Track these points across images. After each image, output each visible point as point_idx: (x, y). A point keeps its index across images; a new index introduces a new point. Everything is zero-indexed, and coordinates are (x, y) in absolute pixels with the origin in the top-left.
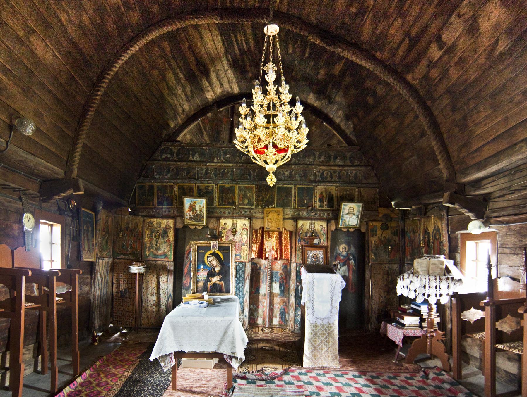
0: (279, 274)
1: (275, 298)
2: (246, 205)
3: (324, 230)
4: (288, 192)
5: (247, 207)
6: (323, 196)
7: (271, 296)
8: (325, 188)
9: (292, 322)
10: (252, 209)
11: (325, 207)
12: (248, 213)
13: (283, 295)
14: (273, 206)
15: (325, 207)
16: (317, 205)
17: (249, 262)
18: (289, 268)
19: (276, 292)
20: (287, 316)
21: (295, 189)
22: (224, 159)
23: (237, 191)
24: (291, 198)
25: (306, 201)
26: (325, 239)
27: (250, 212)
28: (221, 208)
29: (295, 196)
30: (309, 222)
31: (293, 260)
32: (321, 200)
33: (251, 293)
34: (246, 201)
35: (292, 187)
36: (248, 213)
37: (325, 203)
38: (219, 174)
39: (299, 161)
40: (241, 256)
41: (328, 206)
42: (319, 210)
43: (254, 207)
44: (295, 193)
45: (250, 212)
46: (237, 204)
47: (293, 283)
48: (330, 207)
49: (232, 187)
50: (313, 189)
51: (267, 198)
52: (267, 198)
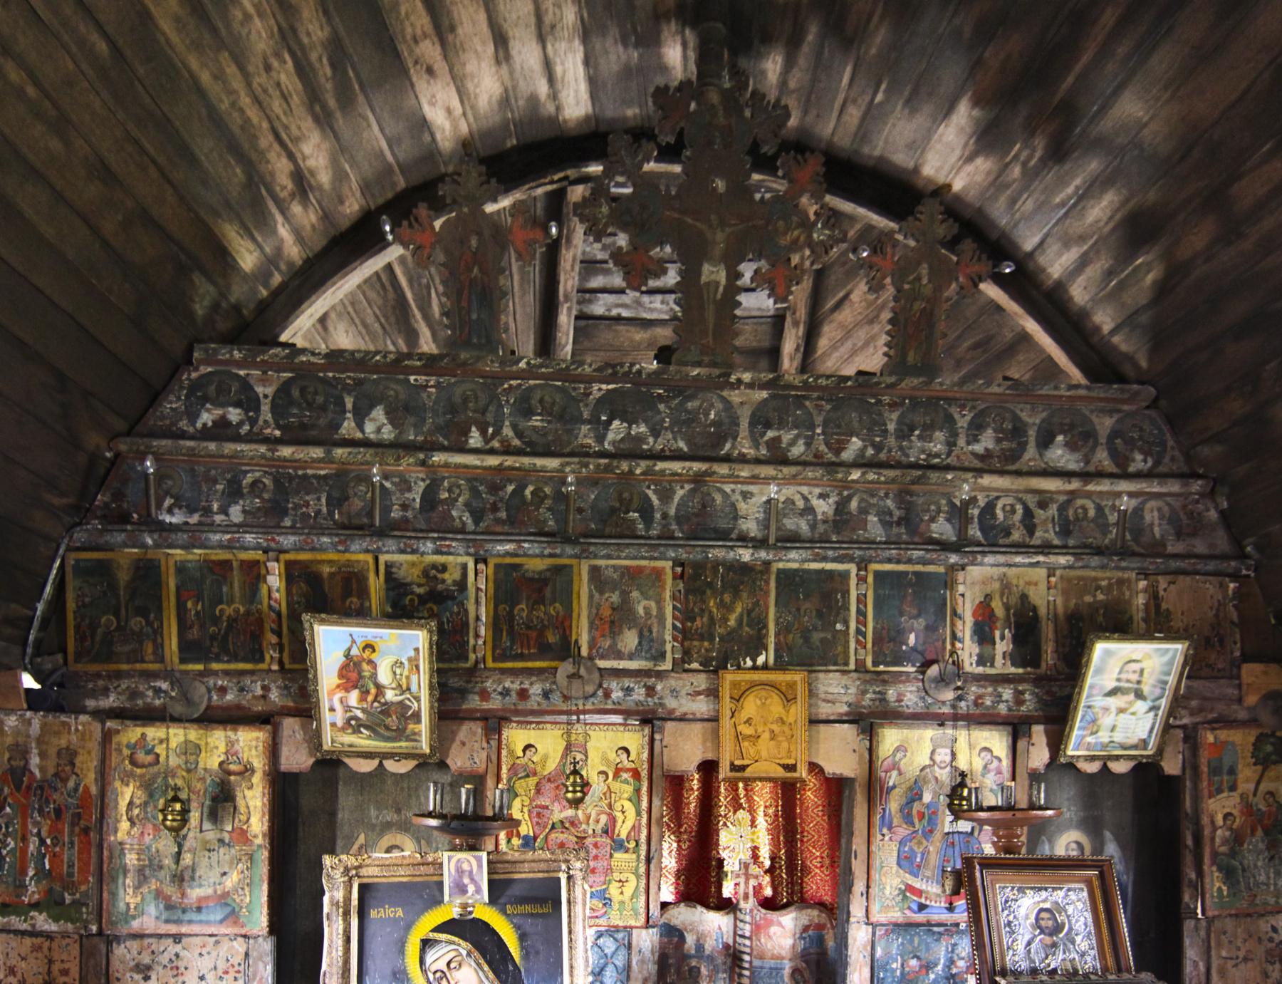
2: (631, 657)
3: (999, 772)
4: (827, 591)
10: (660, 675)
11: (1002, 666)
12: (639, 694)
15: (1002, 666)
23: (583, 587)
24: (846, 623)
27: (651, 691)
28: (503, 671)
29: (861, 613)
31: (857, 910)
32: (983, 635)
34: (630, 640)
37: (1002, 646)
38: (495, 509)
39: (878, 448)
42: (978, 678)
43: (667, 665)
44: (861, 600)
45: (651, 691)
46: (584, 652)
48: (1024, 666)
50: (948, 581)
51: (732, 623)
52: (732, 623)
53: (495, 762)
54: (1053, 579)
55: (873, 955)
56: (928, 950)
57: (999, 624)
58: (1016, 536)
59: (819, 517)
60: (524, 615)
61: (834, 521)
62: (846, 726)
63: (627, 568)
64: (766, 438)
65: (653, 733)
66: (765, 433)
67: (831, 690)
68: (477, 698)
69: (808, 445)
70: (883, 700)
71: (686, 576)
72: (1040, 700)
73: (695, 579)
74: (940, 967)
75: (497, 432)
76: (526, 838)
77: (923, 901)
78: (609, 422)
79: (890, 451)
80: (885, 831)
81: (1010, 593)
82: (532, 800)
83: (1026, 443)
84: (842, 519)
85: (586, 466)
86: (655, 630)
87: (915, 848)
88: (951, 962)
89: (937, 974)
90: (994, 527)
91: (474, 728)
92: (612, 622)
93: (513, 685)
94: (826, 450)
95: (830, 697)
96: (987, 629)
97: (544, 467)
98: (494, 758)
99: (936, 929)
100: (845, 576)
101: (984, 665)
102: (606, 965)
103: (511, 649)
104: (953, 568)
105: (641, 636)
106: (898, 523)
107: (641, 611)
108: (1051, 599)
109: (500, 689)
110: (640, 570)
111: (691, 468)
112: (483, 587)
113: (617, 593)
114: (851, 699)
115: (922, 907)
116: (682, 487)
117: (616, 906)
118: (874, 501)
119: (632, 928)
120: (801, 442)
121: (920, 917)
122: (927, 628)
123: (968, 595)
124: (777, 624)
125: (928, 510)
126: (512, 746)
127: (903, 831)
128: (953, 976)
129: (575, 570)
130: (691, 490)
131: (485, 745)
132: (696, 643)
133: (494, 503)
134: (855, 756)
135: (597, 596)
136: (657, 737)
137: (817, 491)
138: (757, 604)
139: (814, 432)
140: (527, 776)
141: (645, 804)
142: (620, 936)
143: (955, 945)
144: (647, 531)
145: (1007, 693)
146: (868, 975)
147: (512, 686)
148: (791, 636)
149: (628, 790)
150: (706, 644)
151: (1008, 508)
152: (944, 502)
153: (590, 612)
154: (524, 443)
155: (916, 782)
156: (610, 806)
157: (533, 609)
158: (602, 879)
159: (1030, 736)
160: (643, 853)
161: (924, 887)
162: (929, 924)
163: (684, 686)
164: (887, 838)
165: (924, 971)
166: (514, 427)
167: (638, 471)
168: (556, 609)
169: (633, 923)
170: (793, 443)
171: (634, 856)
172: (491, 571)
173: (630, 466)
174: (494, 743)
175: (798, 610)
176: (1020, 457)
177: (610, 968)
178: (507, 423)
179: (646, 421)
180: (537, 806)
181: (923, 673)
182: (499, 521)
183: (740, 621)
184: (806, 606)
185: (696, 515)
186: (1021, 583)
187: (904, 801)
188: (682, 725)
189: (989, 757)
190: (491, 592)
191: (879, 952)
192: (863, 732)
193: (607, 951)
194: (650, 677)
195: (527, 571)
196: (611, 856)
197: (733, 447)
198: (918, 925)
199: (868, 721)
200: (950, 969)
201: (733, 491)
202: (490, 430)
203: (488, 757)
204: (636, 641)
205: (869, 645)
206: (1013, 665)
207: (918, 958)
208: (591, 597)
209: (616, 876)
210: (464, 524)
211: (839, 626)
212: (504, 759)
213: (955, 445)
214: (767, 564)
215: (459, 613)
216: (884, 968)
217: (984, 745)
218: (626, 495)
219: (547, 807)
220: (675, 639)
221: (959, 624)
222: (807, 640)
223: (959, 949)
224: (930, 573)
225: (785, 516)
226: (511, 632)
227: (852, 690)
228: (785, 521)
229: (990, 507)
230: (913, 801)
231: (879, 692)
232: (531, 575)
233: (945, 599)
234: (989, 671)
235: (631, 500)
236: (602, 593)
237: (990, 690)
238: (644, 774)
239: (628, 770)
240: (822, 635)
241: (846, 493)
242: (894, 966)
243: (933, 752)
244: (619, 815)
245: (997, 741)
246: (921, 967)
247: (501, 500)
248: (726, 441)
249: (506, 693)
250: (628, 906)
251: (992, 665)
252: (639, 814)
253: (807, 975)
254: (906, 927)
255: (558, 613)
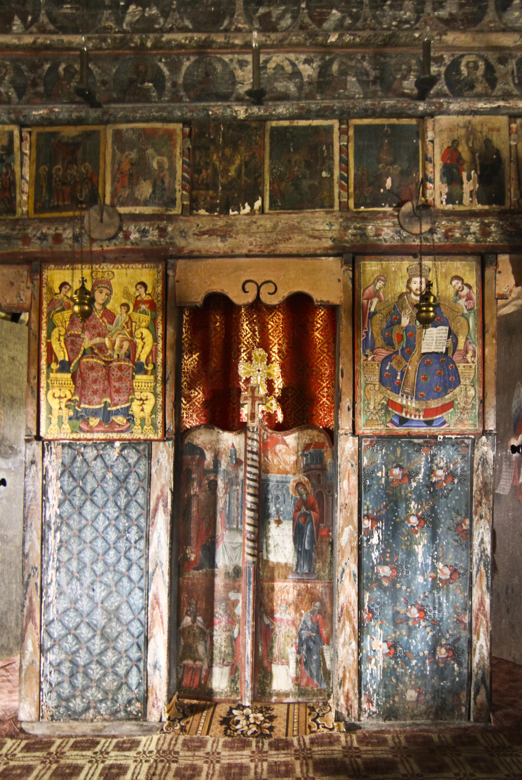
0: (291, 485)
1: (278, 585)
2: (146, 203)
3: (469, 298)
4: (314, 146)
5: (148, 210)
6: (459, 158)
7: (262, 576)
8: (467, 126)
9: (348, 685)
10: (171, 219)
11: (469, 203)
12: (153, 235)
13: (311, 572)
14: (258, 204)
15: (469, 203)
16: (437, 192)
17: (164, 439)
18: (329, 460)
19: (282, 560)
20: (327, 656)
21: (343, 132)
22: (53, 20)
23: (108, 149)
24: (331, 171)
25: (389, 183)
26: (475, 335)
27: (163, 232)
28: (41, 220)
29: (344, 162)
30: (406, 264)
31: (345, 425)
32: (452, 176)
33: (178, 566)
34: (145, 189)
35: (330, 128)
36: (153, 235)
37: (469, 186)
38: (35, 84)
39: (355, 18)
40: (131, 419)
41: (481, 196)
42: (447, 214)
43: (177, 211)
44: (343, 150)
45: (163, 232)
46: (108, 201)
47: (348, 521)
48: (490, 203)
49: (87, 135)
50: (420, 133)
51: (232, 173)
52: (232, 173)
53: (38, 298)
54: (514, 126)
55: (360, 464)
56: (409, 459)
57: (465, 166)
58: (479, 88)
59: (306, 80)
60: (60, 173)
61: (318, 83)
62: (331, 259)
63: (144, 130)
64: (258, 15)
65: (166, 269)
66: (257, 10)
67: (317, 227)
68: (20, 243)
69: (294, 18)
70: (364, 235)
71: (193, 134)
72: (505, 232)
73: (201, 136)
74: (421, 476)
75: (35, 19)
76: (63, 362)
77: (404, 415)
78: (126, 7)
79: (365, 20)
80: (368, 352)
81: (475, 138)
82: (67, 331)
83: (486, 7)
84: (324, 83)
85: (105, 40)
86: (167, 181)
87: (395, 367)
88: (430, 472)
89: (418, 482)
90: (459, 82)
91: (21, 271)
92: (131, 175)
93: (49, 230)
94: (310, 22)
95: (316, 233)
96: (455, 170)
97: (70, 43)
98: (37, 295)
99: (416, 441)
100: (329, 130)
101: (454, 203)
102: (130, 473)
103: (50, 202)
104: (422, 117)
105: (154, 186)
106: (374, 82)
107: (155, 165)
108: (513, 143)
109: (38, 235)
110: (154, 131)
111: (192, 38)
112: (27, 152)
113: (135, 151)
114: (335, 234)
115: (403, 421)
116: (188, 59)
117: (138, 422)
118: (353, 63)
119: (151, 441)
120: (288, 16)
121: (401, 430)
122: (402, 173)
123: (436, 141)
124: (271, 174)
125: (400, 70)
126: (51, 284)
127: (384, 353)
128: (433, 484)
129: (102, 134)
130: (196, 62)
131: (29, 285)
132: (202, 192)
133: (34, 79)
134: (340, 286)
135: (118, 154)
136: (170, 273)
137: (303, 57)
138: (253, 156)
139: (299, 7)
140: (63, 310)
141: (160, 332)
142: (141, 447)
143: (434, 455)
144: (160, 98)
145: (474, 226)
146: (356, 482)
147: (48, 232)
148: (283, 185)
149: (146, 319)
150: (211, 192)
151: (471, 65)
152: (414, 62)
153: (113, 167)
154: (56, 27)
155: (394, 308)
156: (131, 334)
157: (67, 168)
158: (126, 397)
159: (497, 265)
160: (160, 375)
161: (404, 402)
162: (409, 436)
163: (190, 228)
164: (370, 358)
165: (406, 480)
166: (49, 14)
167: (149, 44)
168: (85, 168)
169: (152, 436)
170: (281, 17)
171: (152, 377)
172: (34, 137)
173: (141, 39)
174: (36, 283)
175: (289, 161)
176: (480, 20)
177: (133, 476)
178: (43, 12)
179: (157, 5)
180: (71, 335)
181: (398, 211)
182: (37, 94)
183: (239, 171)
184: (296, 157)
185: (201, 83)
186: (485, 129)
187: (385, 325)
188: (190, 262)
189: (460, 284)
190: (34, 155)
191: (365, 461)
192: (346, 263)
193: (131, 461)
194: (162, 220)
195: (63, 137)
196: (133, 378)
197: (231, 23)
198: (399, 437)
199: (353, 253)
200: (430, 478)
201: (231, 60)
202: (30, 18)
203: (32, 295)
204: (150, 190)
205: (351, 190)
206: (479, 202)
207: (401, 468)
208: (114, 155)
209: (137, 395)
210: (9, 98)
211: (324, 174)
212: (44, 296)
213: (423, 12)
214: (262, 120)
215: (7, 173)
216: (371, 475)
217: (454, 274)
218: (142, 68)
219: (79, 336)
220: (183, 188)
221: (430, 166)
222: (297, 186)
223: (437, 460)
224: (403, 126)
225: (276, 80)
226: (50, 189)
227: (336, 227)
228: (276, 84)
229: (455, 65)
230: (394, 325)
231: (360, 228)
232: (65, 140)
233: (418, 147)
234: (458, 208)
235: (146, 72)
236: (122, 151)
237: (459, 223)
238: (159, 305)
239: (145, 302)
240: (311, 182)
241: (327, 58)
242: (379, 474)
243: (409, 281)
244: (139, 341)
245: (466, 270)
246: (403, 475)
247: (39, 77)
248: (224, 18)
249: (43, 237)
250: (148, 421)
251: (461, 203)
252: (155, 340)
253: (309, 488)
254: (388, 439)
255: (87, 171)
